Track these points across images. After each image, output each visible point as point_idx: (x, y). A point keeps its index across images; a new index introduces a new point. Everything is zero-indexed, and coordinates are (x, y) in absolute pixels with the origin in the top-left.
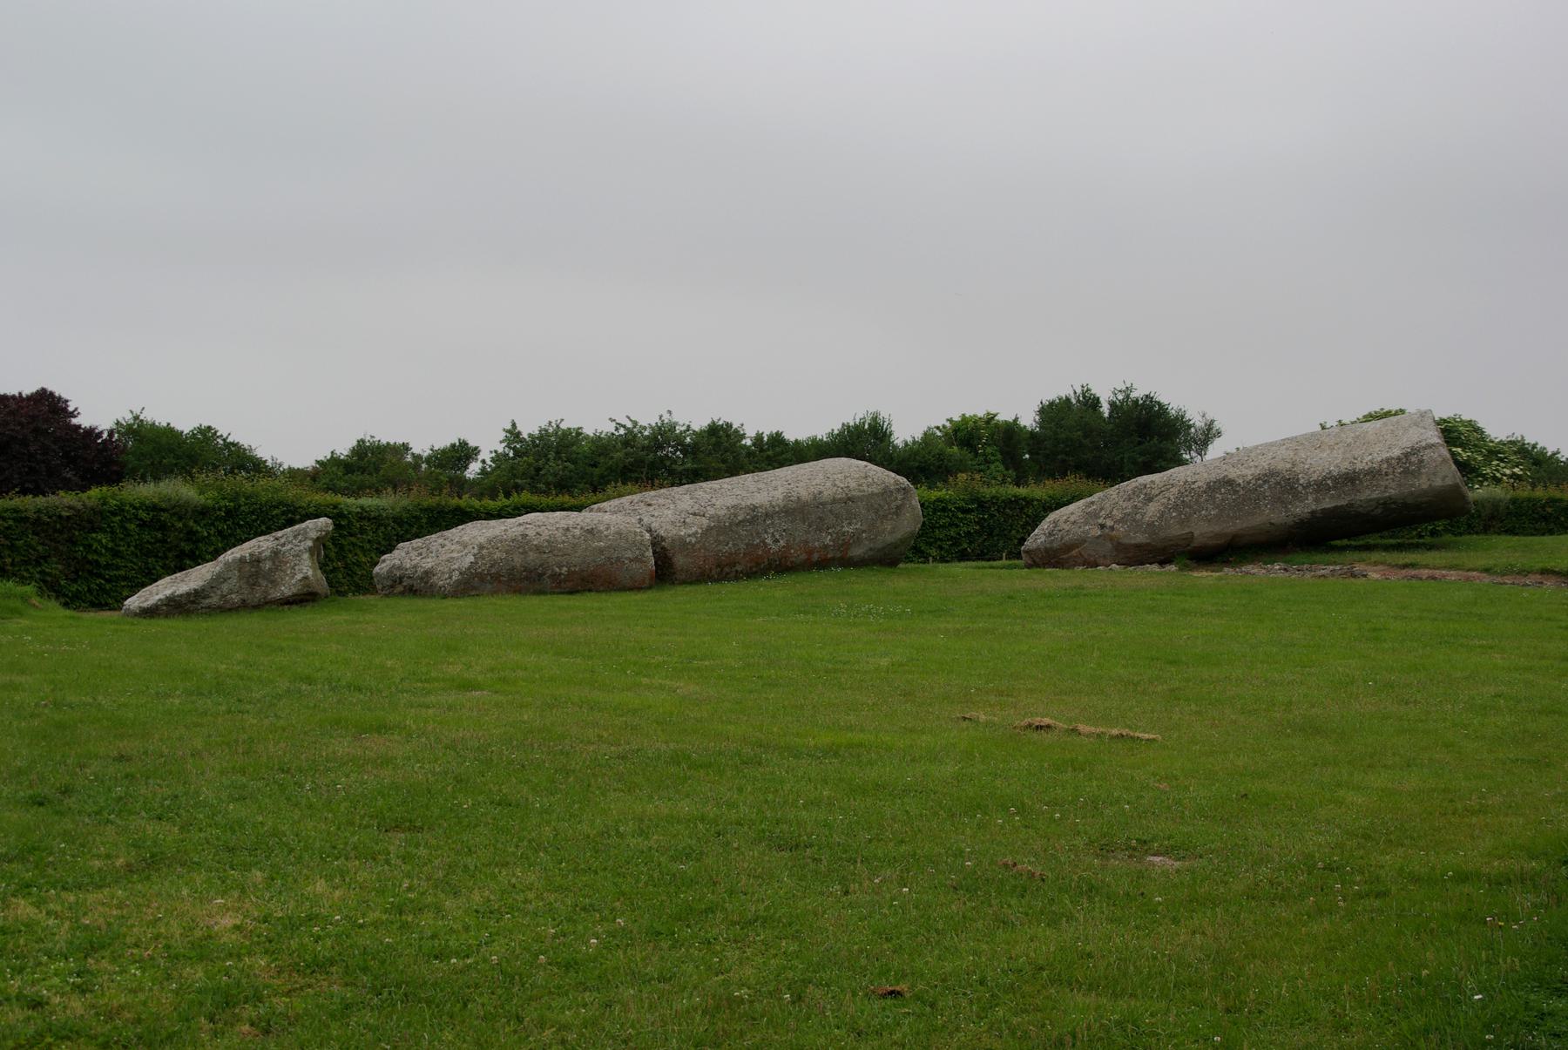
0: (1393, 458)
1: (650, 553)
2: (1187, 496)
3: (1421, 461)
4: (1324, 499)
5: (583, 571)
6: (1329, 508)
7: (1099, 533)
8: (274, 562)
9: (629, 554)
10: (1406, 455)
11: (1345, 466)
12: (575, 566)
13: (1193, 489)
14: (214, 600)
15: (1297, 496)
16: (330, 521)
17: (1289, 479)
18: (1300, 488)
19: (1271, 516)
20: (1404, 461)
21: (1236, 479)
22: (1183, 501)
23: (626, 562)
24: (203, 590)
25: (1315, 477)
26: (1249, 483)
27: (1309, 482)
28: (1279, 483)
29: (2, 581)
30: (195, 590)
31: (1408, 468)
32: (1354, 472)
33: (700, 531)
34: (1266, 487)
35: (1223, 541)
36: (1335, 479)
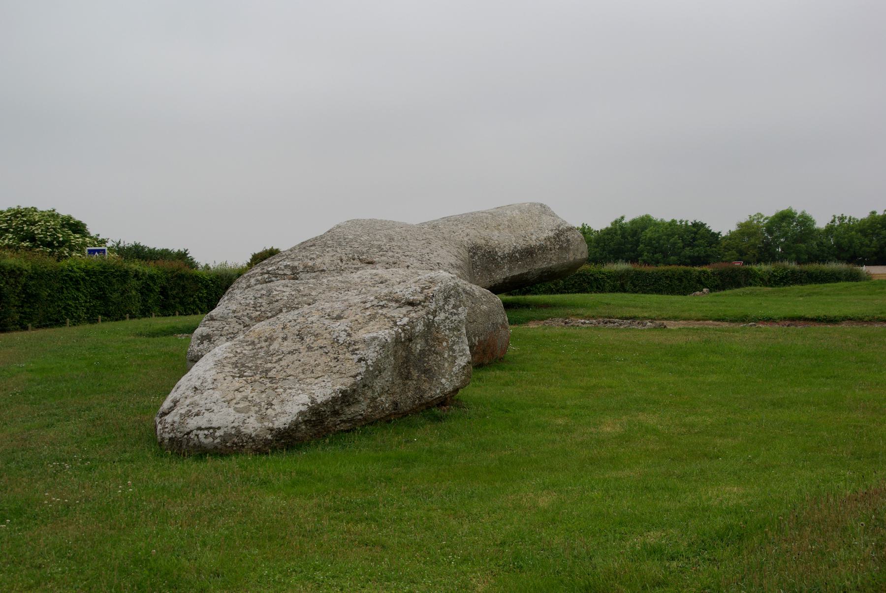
3: (568, 241)
4: (514, 268)
6: (516, 276)
8: (427, 341)
10: (558, 235)
14: (361, 408)
17: (490, 252)
18: (499, 259)
24: (354, 391)
25: (507, 251)
27: (504, 255)
30: (343, 392)
31: (562, 245)
32: (531, 247)
36: (520, 253)
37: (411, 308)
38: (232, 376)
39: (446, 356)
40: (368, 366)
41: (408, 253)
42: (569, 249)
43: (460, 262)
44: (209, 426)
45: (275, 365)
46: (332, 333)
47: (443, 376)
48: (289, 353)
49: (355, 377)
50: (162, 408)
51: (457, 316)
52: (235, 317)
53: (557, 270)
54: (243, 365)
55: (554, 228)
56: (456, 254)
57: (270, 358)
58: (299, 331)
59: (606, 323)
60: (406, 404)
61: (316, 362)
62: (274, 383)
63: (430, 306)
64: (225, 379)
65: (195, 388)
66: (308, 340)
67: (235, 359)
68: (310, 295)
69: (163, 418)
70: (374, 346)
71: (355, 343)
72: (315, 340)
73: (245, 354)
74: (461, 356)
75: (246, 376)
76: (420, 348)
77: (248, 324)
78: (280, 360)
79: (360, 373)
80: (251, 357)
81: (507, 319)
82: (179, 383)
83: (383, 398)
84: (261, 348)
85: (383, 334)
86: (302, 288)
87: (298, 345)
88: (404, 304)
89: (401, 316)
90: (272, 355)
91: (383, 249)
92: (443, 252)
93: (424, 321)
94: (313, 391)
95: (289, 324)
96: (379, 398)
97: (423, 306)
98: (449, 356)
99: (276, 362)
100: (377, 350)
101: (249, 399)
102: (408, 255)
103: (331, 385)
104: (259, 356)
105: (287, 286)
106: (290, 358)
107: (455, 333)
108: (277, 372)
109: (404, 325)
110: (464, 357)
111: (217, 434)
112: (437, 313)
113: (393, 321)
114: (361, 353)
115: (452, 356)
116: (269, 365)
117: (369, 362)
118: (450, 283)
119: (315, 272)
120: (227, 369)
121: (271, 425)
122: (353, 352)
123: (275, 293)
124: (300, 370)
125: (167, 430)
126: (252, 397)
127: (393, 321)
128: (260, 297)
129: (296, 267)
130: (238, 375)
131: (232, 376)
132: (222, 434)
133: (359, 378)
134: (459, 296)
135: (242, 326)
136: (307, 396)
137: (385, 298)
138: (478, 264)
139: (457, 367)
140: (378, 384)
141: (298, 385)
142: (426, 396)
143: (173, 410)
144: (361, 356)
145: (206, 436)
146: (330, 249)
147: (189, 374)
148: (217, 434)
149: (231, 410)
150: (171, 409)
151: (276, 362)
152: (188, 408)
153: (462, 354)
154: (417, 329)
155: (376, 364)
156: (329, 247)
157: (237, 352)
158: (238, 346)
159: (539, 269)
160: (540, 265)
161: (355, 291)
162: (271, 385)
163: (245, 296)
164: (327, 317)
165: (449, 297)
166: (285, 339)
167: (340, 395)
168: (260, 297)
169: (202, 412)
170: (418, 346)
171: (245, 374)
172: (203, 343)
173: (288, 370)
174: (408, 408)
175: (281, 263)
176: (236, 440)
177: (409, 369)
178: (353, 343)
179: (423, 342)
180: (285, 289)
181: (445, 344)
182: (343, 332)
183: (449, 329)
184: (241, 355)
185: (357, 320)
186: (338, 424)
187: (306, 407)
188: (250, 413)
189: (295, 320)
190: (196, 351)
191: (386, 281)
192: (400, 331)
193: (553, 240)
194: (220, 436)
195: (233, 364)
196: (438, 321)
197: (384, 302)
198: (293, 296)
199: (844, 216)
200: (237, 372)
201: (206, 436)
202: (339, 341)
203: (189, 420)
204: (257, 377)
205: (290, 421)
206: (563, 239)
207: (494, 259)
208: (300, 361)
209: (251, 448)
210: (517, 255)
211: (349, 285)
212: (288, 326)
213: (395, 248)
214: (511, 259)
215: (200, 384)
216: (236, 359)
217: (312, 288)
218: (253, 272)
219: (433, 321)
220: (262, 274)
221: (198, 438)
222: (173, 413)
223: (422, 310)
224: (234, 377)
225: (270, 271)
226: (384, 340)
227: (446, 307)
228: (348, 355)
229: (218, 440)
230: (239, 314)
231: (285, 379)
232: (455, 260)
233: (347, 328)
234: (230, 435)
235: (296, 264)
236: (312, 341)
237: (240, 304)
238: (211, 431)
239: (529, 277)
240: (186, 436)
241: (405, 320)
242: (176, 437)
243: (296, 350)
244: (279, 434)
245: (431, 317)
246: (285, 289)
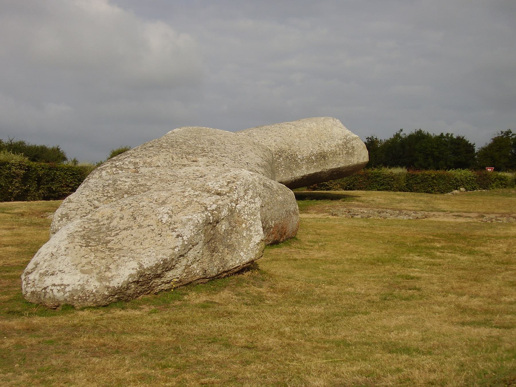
3: (353, 147)
4: (311, 168)
6: (312, 174)
8: (230, 223)
10: (345, 143)
11: (316, 150)
17: (292, 155)
18: (299, 161)
20: (345, 146)
27: (303, 157)
28: (287, 157)
30: (165, 261)
31: (348, 151)
34: (281, 159)
36: (316, 157)
37: (219, 197)
38: (80, 245)
39: (244, 235)
40: (184, 241)
41: (225, 155)
42: (354, 154)
43: (265, 162)
44: (61, 283)
45: (113, 238)
46: (158, 215)
47: (242, 250)
48: (124, 229)
49: (173, 249)
50: (26, 269)
51: (254, 204)
52: (87, 200)
53: (344, 171)
54: (89, 238)
55: (343, 138)
56: (262, 156)
57: (110, 233)
58: (133, 213)
59: (380, 213)
60: (213, 271)
61: (144, 237)
62: (112, 252)
63: (233, 196)
64: (75, 248)
65: (52, 254)
66: (139, 219)
67: (83, 233)
68: (146, 185)
69: (27, 277)
70: (189, 226)
71: (175, 223)
72: (144, 220)
73: (91, 229)
74: (257, 235)
75: (91, 246)
76: (224, 228)
77: (97, 206)
78: (117, 234)
79: (178, 246)
80: (96, 231)
81: (298, 208)
82: (40, 250)
83: (195, 265)
84: (104, 224)
85: (196, 217)
86: (140, 179)
87: (132, 223)
88: (214, 194)
89: (211, 203)
90: (112, 230)
91: (205, 151)
92: (252, 155)
93: (228, 207)
94: (141, 259)
95: (126, 207)
96: (192, 266)
97: (228, 196)
98: (247, 234)
99: (114, 236)
100: (191, 229)
101: (92, 263)
102: (224, 156)
103: (155, 255)
104: (101, 231)
105: (129, 178)
106: (125, 233)
107: (252, 217)
108: (115, 243)
109: (213, 210)
110: (258, 236)
111: (67, 289)
112: (239, 202)
113: (205, 207)
114: (179, 231)
115: (249, 235)
116: (109, 238)
117: (185, 238)
118: (249, 179)
119: (152, 167)
120: (77, 240)
121: (108, 284)
122: (173, 230)
123: (119, 182)
124: (132, 242)
125: (29, 285)
126: (95, 262)
127: (205, 207)
128: (108, 186)
129: (137, 163)
130: (85, 245)
131: (80, 245)
132: (71, 289)
133: (176, 250)
134: (256, 189)
135: (92, 208)
136: (136, 263)
137: (200, 189)
138: (282, 164)
139: (253, 243)
140: (191, 254)
141: (129, 254)
142: (228, 265)
143: (35, 270)
144: (179, 233)
145: (59, 291)
146: (164, 150)
147: (48, 243)
148: (67, 289)
149: (78, 271)
150: (33, 269)
151: (114, 236)
152: (46, 269)
153: (257, 233)
154: (223, 214)
155: (190, 240)
156: (163, 148)
157: (85, 227)
158: (86, 223)
159: (331, 169)
160: (330, 166)
161: (180, 183)
162: (109, 253)
163: (96, 185)
164: (154, 202)
165: (248, 190)
166: (122, 218)
167: (162, 262)
168: (108, 186)
169: (56, 272)
170: (223, 226)
171: (90, 244)
172: (62, 220)
173: (122, 242)
174: (214, 274)
175: (126, 159)
176: (81, 295)
177: (216, 244)
178: (173, 223)
179: (227, 223)
180: (127, 180)
181: (244, 225)
182: (166, 215)
183: (247, 214)
184: (88, 229)
185: (177, 206)
186: (160, 285)
187: (135, 270)
188: (92, 274)
189: (130, 204)
190: (56, 226)
191: (205, 176)
192: (209, 214)
193: (341, 147)
194: (69, 291)
195: (81, 236)
196: (239, 208)
197: (198, 192)
198: (133, 185)
200: (84, 243)
201: (59, 291)
202: (163, 221)
203: (46, 278)
204: (99, 247)
205: (122, 281)
206: (349, 146)
207: (295, 161)
208: (132, 235)
209: (92, 301)
210: (313, 158)
211: (176, 178)
212: (124, 208)
213: (214, 150)
214: (308, 161)
215: (55, 251)
216: (84, 232)
217: (147, 180)
218: (104, 166)
219: (235, 207)
220: (111, 167)
221: (52, 292)
222: (34, 273)
223: (227, 199)
224: (81, 246)
225: (117, 165)
226: (196, 221)
228: (169, 232)
229: (68, 294)
230: (91, 199)
231: (121, 249)
232: (260, 161)
233: (169, 212)
234: (77, 290)
235: (137, 160)
236: (142, 221)
237: (92, 190)
238: (63, 287)
239: (322, 175)
240: (44, 290)
241: (214, 206)
242: (36, 291)
243: (130, 227)
244: (114, 291)
246: (127, 180)
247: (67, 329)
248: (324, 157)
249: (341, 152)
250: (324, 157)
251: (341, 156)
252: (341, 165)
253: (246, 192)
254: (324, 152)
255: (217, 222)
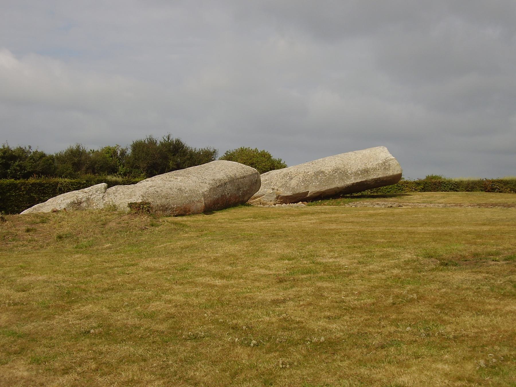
0: (380, 164)
1: (203, 199)
2: (307, 177)
3: (390, 165)
5: (182, 206)
7: (272, 192)
8: (87, 203)
9: (197, 200)
10: (384, 163)
11: (363, 167)
12: (179, 204)
13: (309, 174)
15: (348, 177)
16: (105, 184)
17: (345, 171)
19: (338, 184)
20: (384, 165)
21: (325, 171)
22: (306, 179)
23: (196, 202)
26: (330, 172)
27: (352, 172)
29: (1, 211)
33: (208, 189)
35: (318, 195)
36: (361, 171)
179: (86, 203)
181: (94, 204)
199: (280, 159)
227: (96, 194)
245: (90, 196)
247: (394, 284)
248: (367, 172)
249: (380, 168)
250: (367, 172)
251: (380, 170)
252: (380, 176)
253: (96, 192)
254: (367, 169)
255: (81, 203)
